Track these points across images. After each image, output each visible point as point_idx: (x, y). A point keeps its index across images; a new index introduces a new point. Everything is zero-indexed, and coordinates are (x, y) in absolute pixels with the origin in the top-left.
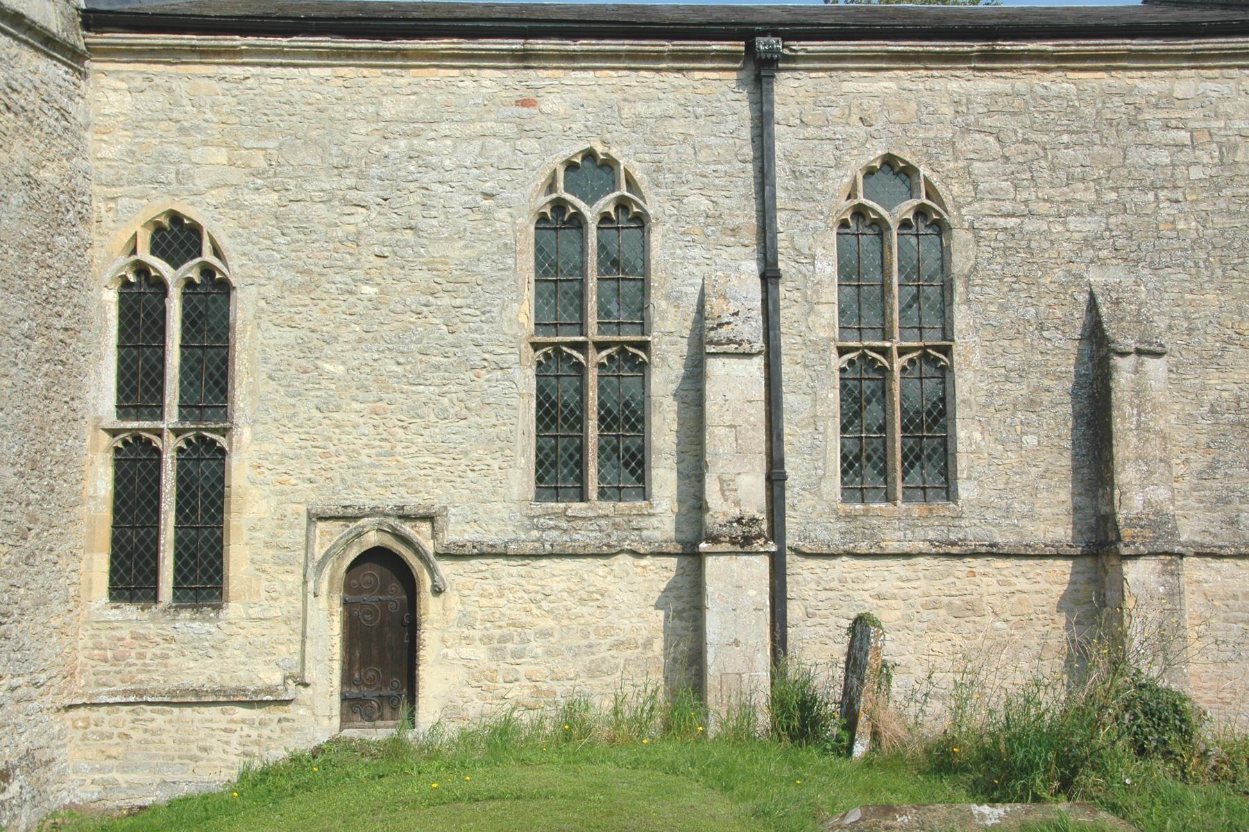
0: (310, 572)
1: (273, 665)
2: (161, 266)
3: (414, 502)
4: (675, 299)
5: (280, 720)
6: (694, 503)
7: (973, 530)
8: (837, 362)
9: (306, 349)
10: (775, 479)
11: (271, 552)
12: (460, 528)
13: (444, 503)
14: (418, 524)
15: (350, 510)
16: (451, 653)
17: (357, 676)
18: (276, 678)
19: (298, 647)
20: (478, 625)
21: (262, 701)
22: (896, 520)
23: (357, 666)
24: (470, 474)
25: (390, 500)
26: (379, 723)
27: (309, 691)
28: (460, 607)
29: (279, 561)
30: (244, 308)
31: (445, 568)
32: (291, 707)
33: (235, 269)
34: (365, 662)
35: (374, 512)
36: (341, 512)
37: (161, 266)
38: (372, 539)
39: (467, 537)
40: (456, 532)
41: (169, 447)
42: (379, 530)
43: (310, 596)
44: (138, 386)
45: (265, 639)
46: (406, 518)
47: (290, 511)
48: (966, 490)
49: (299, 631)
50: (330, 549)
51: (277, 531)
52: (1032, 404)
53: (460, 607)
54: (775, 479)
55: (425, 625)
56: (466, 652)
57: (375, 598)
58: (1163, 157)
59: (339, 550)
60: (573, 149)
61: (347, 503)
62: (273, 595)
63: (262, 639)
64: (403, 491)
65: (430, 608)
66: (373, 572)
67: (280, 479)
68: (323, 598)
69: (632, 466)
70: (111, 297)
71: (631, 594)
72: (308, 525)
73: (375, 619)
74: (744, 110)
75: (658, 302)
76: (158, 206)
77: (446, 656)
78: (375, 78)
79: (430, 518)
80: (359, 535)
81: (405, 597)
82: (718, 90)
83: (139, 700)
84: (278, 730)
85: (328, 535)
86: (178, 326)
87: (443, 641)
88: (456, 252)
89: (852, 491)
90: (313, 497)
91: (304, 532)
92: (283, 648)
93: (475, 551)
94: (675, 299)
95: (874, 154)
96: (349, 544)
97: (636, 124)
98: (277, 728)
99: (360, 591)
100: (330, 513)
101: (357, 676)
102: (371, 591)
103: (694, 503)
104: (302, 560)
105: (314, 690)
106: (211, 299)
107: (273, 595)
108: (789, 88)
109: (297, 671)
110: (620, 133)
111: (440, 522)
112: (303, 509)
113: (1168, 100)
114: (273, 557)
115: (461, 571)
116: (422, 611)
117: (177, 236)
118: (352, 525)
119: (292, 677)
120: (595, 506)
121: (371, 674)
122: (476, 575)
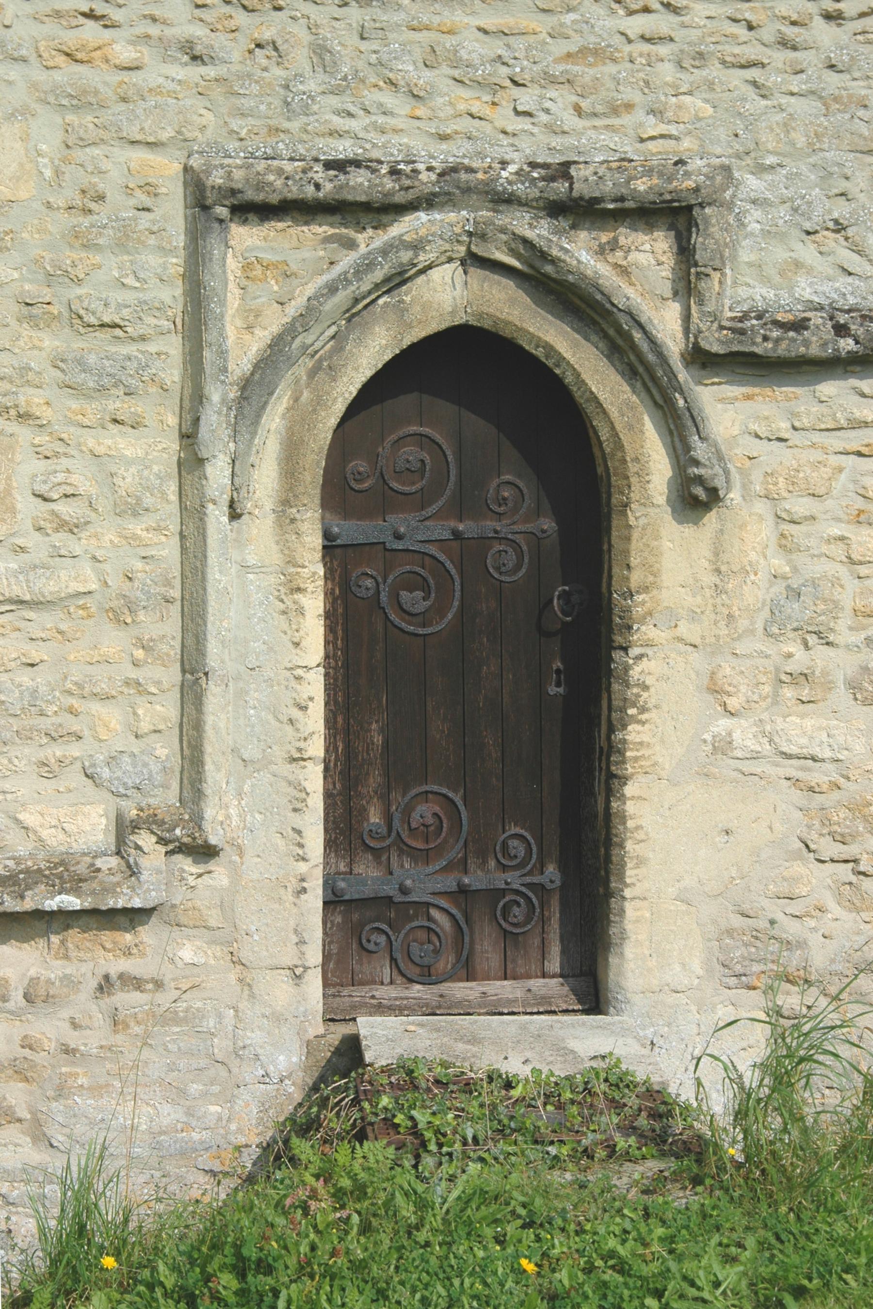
0: (214, 421)
1: (74, 778)
3: (603, 149)
5: (105, 986)
11: (50, 342)
12: (780, 254)
13: (721, 150)
14: (626, 236)
15: (359, 178)
16: (743, 734)
17: (375, 818)
18: (87, 827)
19: (166, 710)
20: (844, 632)
21: (39, 914)
23: (374, 780)
24: (823, 33)
25: (510, 143)
26: (461, 990)
27: (219, 874)
28: (779, 563)
29: (77, 380)
31: (727, 412)
32: (147, 934)
34: (404, 766)
35: (453, 187)
36: (328, 186)
38: (445, 296)
39: (805, 290)
40: (768, 271)
42: (474, 261)
43: (217, 515)
45: (41, 679)
46: (578, 210)
47: (116, 175)
49: (172, 648)
50: (289, 332)
51: (69, 256)
53: (779, 563)
55: (645, 631)
56: (801, 730)
57: (441, 530)
59: (318, 337)
61: (343, 149)
62: (64, 508)
63: (25, 678)
64: (560, 102)
65: (667, 566)
66: (428, 428)
67: (70, 39)
68: (261, 525)
72: (196, 238)
73: (440, 610)
77: (722, 747)
79: (676, 215)
80: (398, 280)
81: (548, 524)
84: (99, 1019)
85: (272, 277)
87: (715, 689)
90: (206, 122)
91: (176, 264)
92: (112, 716)
93: (847, 345)
96: (356, 313)
98: (96, 1013)
99: (382, 501)
100: (279, 189)
101: (375, 818)
102: (422, 500)
104: (173, 374)
105: (235, 873)
107: (64, 508)
109: (166, 798)
111: (691, 223)
112: (167, 169)
114: (58, 362)
115: (783, 427)
116: (636, 578)
118: (369, 241)
119: (149, 821)
121: (424, 812)
122: (836, 441)
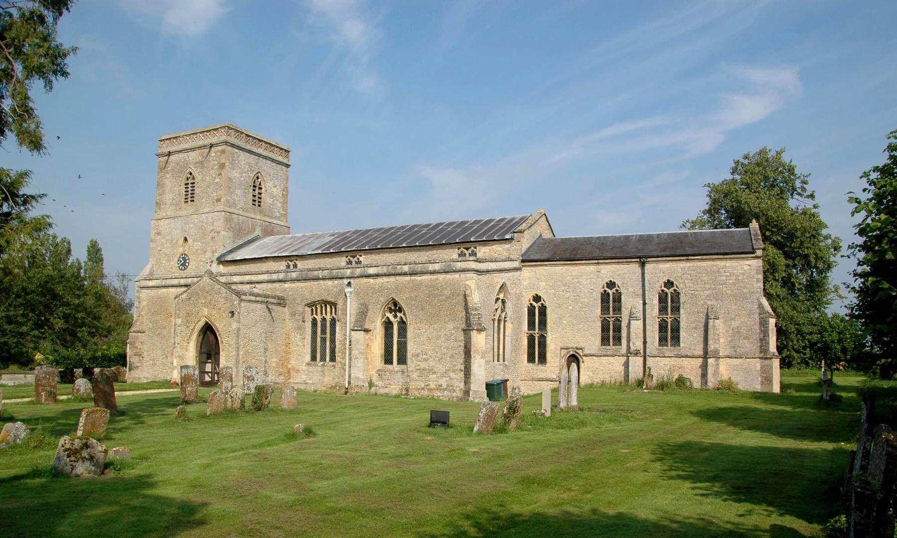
2: (534, 303)
3: (579, 346)
4: (626, 309)
6: (629, 347)
7: (683, 352)
8: (657, 320)
9: (560, 319)
10: (645, 343)
22: (668, 350)
25: (575, 346)
30: (548, 311)
31: (584, 358)
33: (547, 304)
37: (534, 303)
38: (572, 353)
41: (537, 336)
44: (531, 325)
48: (682, 344)
52: (696, 328)
54: (645, 343)
58: (724, 278)
60: (607, 280)
66: (572, 358)
69: (618, 340)
70: (526, 309)
71: (617, 364)
74: (640, 271)
75: (623, 309)
76: (533, 294)
78: (571, 268)
82: (635, 267)
83: (533, 380)
85: (564, 352)
86: (538, 316)
88: (586, 300)
89: (660, 345)
94: (626, 309)
95: (665, 279)
97: (619, 275)
103: (629, 347)
106: (543, 311)
108: (648, 267)
110: (616, 277)
113: (725, 267)
117: (537, 298)
120: (611, 347)
